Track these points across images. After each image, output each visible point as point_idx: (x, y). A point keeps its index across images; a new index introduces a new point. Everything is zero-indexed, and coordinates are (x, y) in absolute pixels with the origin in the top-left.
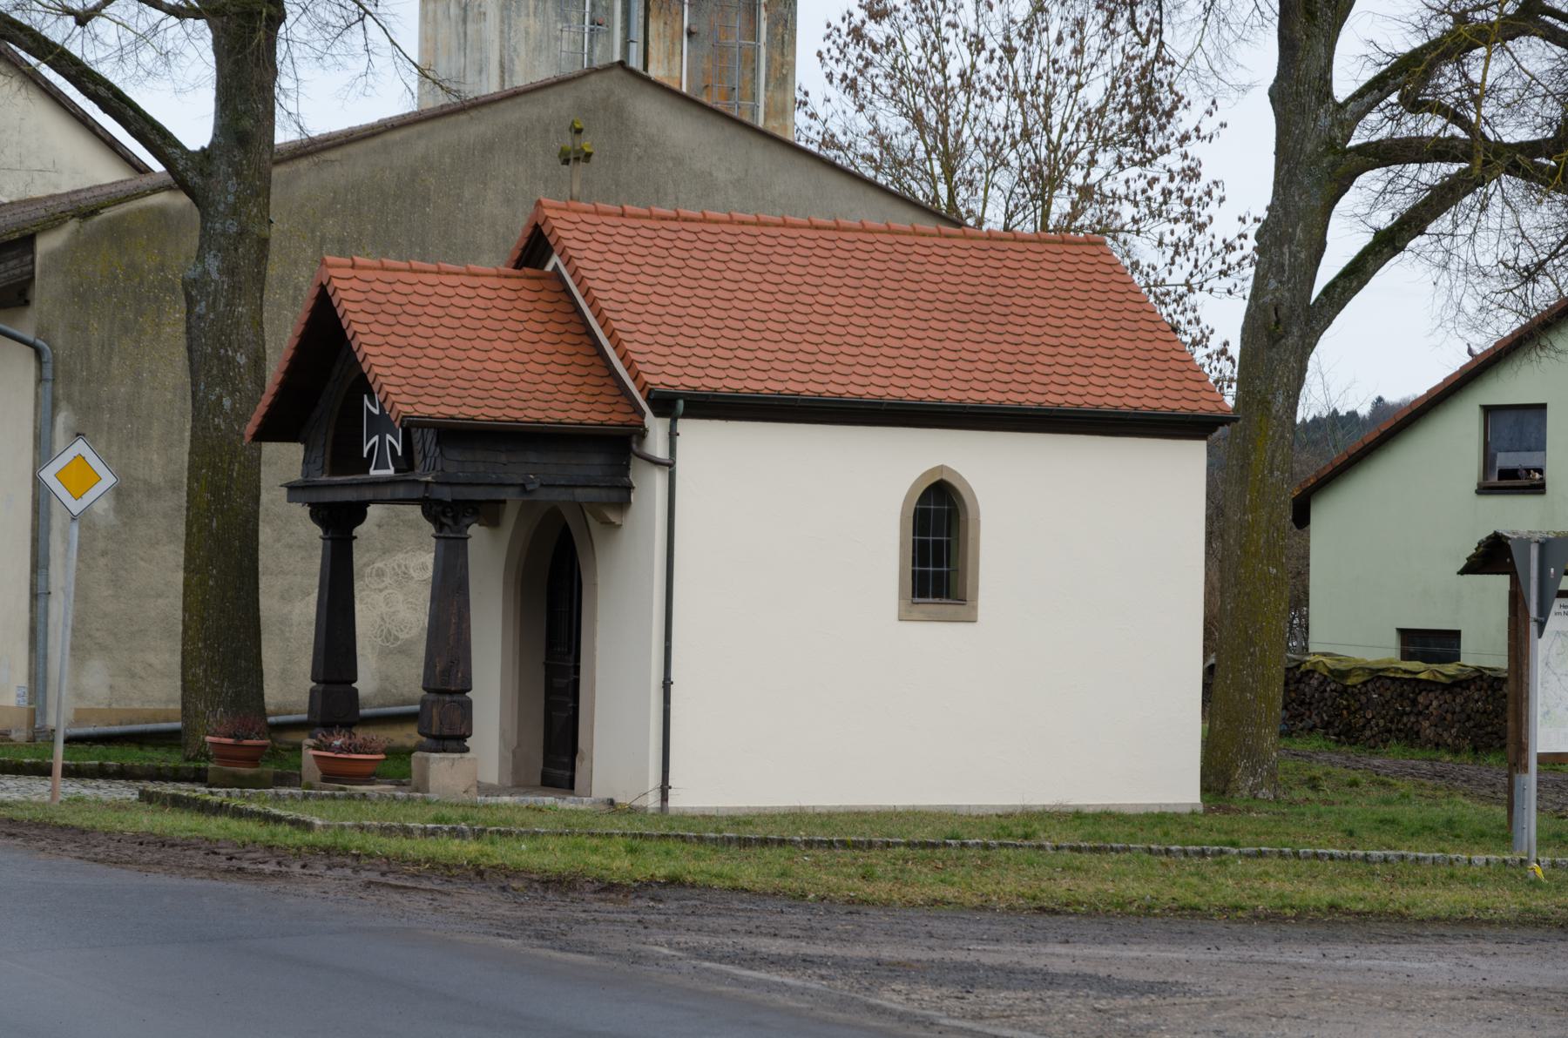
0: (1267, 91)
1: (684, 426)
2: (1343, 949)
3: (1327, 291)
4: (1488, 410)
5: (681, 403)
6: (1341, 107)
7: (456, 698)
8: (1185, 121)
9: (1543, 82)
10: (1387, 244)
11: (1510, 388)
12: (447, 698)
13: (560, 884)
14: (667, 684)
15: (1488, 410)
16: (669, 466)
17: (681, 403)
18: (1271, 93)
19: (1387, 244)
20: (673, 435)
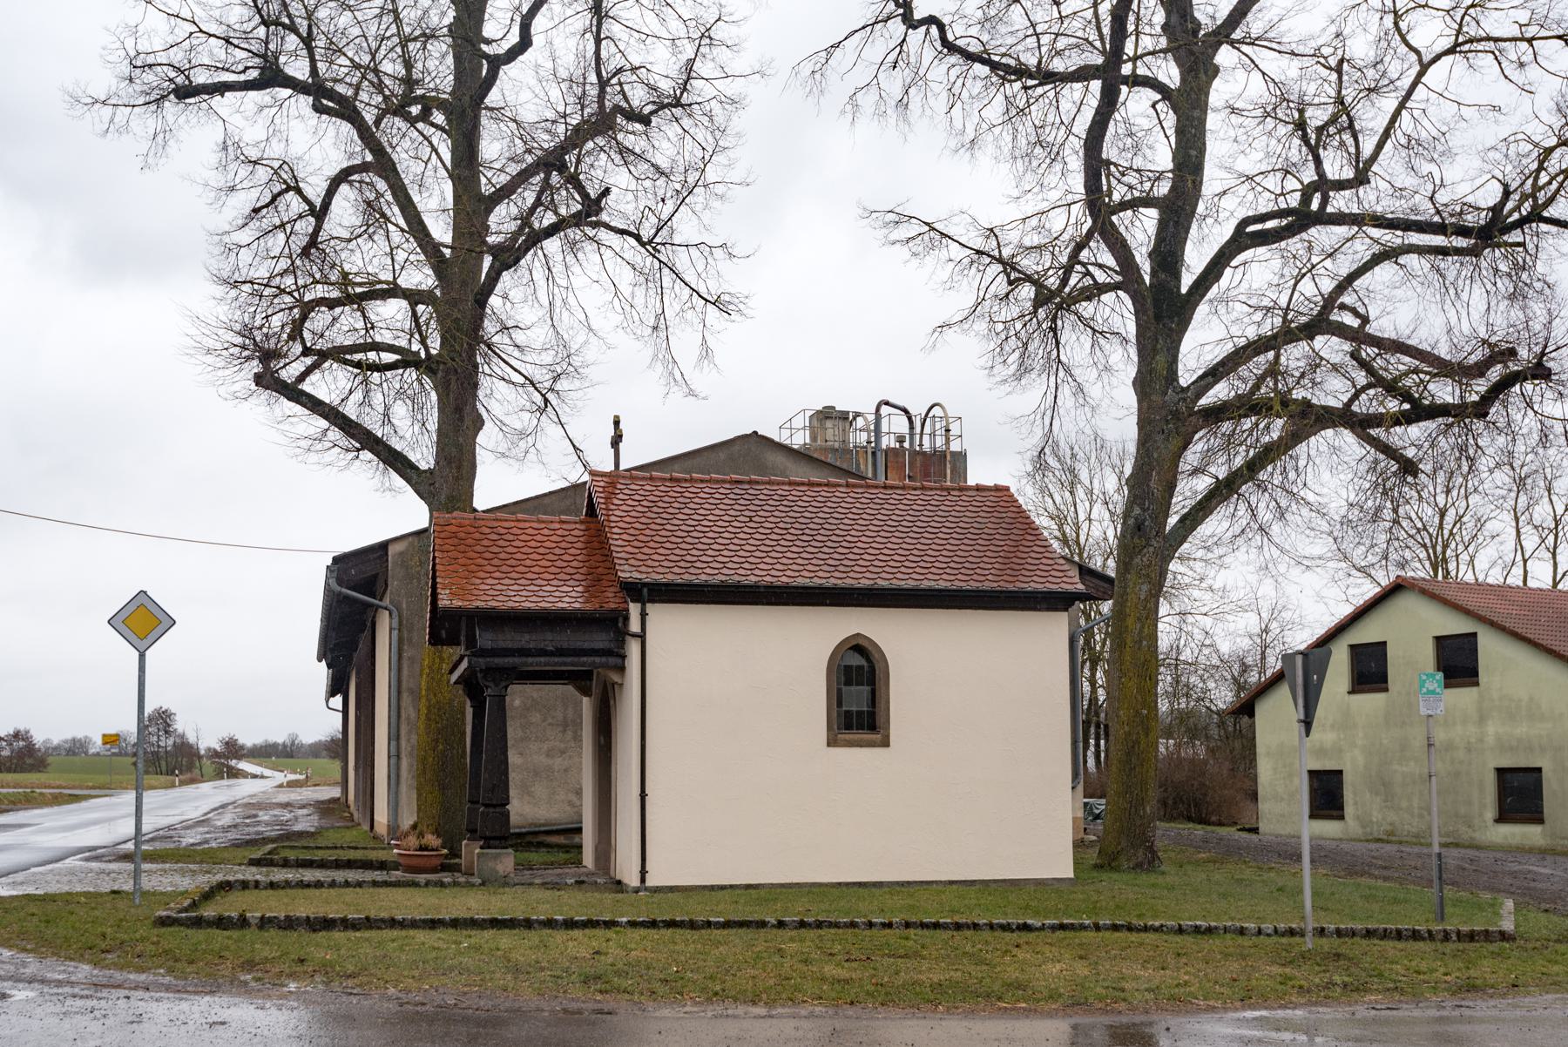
0: (1130, 382)
1: (650, 607)
2: (225, 1000)
3: (1183, 520)
4: (1352, 647)
5: (645, 590)
6: (1184, 390)
7: (498, 810)
8: (1251, 568)
9: (1431, 530)
10: (1223, 491)
11: (1366, 634)
12: (491, 810)
13: (1472, 936)
14: (643, 795)
15: (1352, 647)
16: (642, 637)
17: (645, 590)
18: (1134, 383)
19: (1223, 491)
20: (643, 615)
